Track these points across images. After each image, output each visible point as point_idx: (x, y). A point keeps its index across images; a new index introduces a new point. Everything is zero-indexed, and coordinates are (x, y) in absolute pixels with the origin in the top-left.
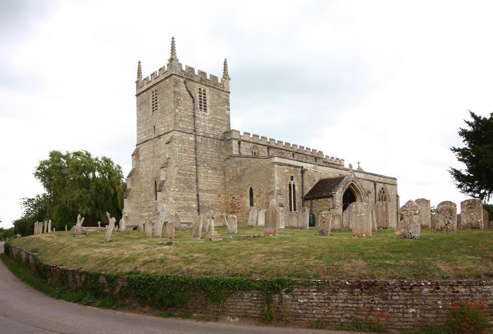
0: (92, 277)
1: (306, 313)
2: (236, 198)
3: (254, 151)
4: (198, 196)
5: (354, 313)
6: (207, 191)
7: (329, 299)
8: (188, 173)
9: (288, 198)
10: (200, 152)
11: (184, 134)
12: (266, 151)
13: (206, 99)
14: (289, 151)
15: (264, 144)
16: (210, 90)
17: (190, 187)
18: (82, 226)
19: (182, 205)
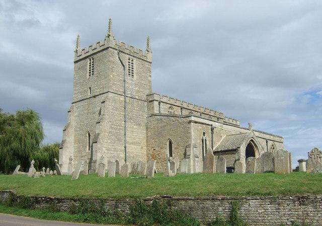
0: (83, 201)
1: (264, 219)
2: (156, 150)
3: (170, 111)
4: (125, 147)
5: (295, 218)
6: (133, 143)
7: (279, 209)
8: (118, 127)
9: (201, 150)
10: (128, 110)
13: (134, 67)
16: (137, 60)
17: (119, 140)
19: (113, 155)
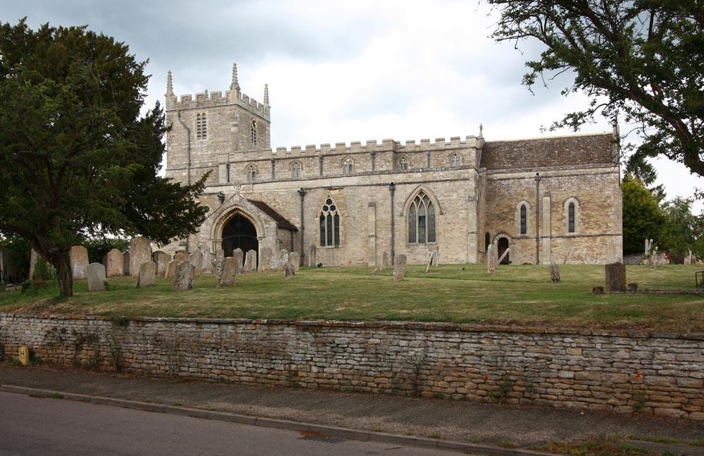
9: (341, 228)
11: (177, 171)
12: (271, 166)
14: (313, 157)
15: (265, 158)
16: (210, 112)
18: (90, 263)
